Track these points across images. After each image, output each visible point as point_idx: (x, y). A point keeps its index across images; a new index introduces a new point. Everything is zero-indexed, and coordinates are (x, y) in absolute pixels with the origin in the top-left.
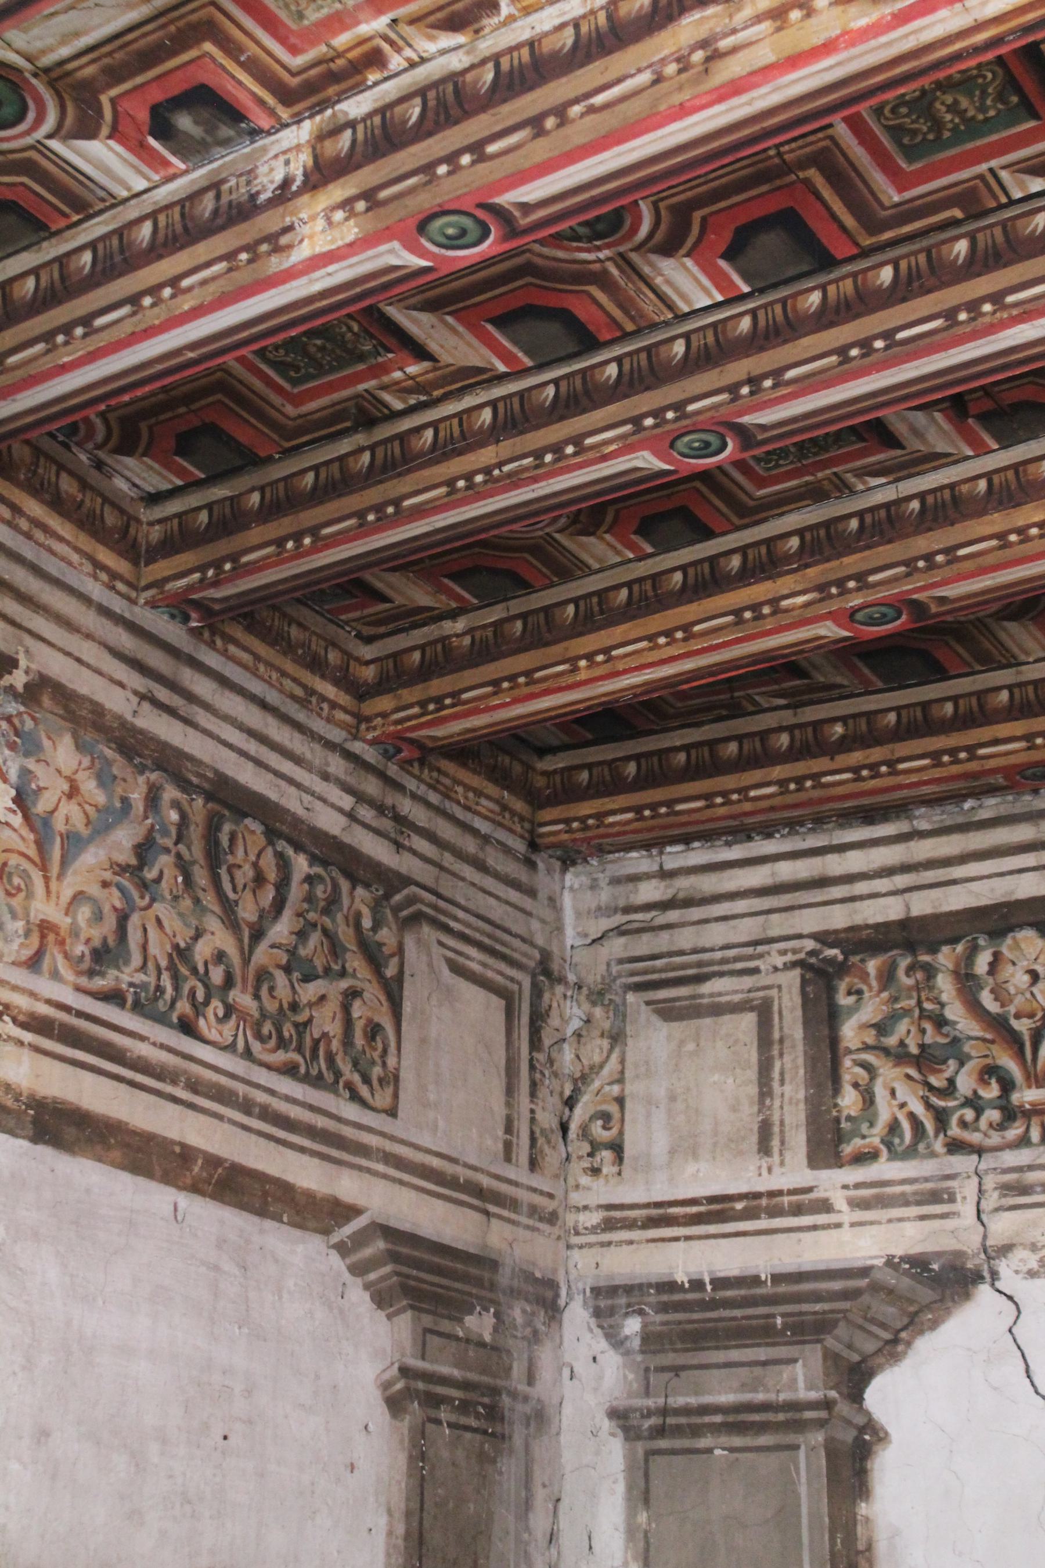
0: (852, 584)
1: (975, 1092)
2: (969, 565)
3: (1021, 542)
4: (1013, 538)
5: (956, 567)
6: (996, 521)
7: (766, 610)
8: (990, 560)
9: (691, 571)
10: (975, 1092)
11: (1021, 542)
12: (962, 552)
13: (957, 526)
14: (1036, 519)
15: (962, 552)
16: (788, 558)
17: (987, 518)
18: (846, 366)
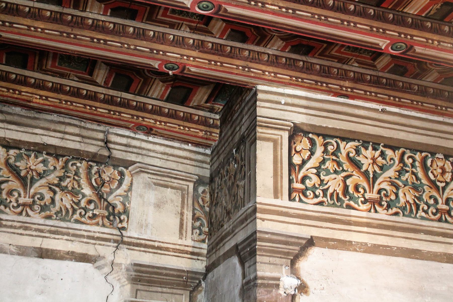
0: (65, 34)
1: (86, 206)
2: (16, 30)
3: (34, 31)
4: (32, 29)
5: (11, 29)
6: (28, 22)
7: (444, 108)
8: (23, 32)
9: (75, 18)
10: (86, 206)
11: (34, 31)
12: (15, 25)
13: (15, 17)
14: (41, 27)
15: (15, 25)
16: (188, 45)
17: (26, 19)
18: (312, 19)
